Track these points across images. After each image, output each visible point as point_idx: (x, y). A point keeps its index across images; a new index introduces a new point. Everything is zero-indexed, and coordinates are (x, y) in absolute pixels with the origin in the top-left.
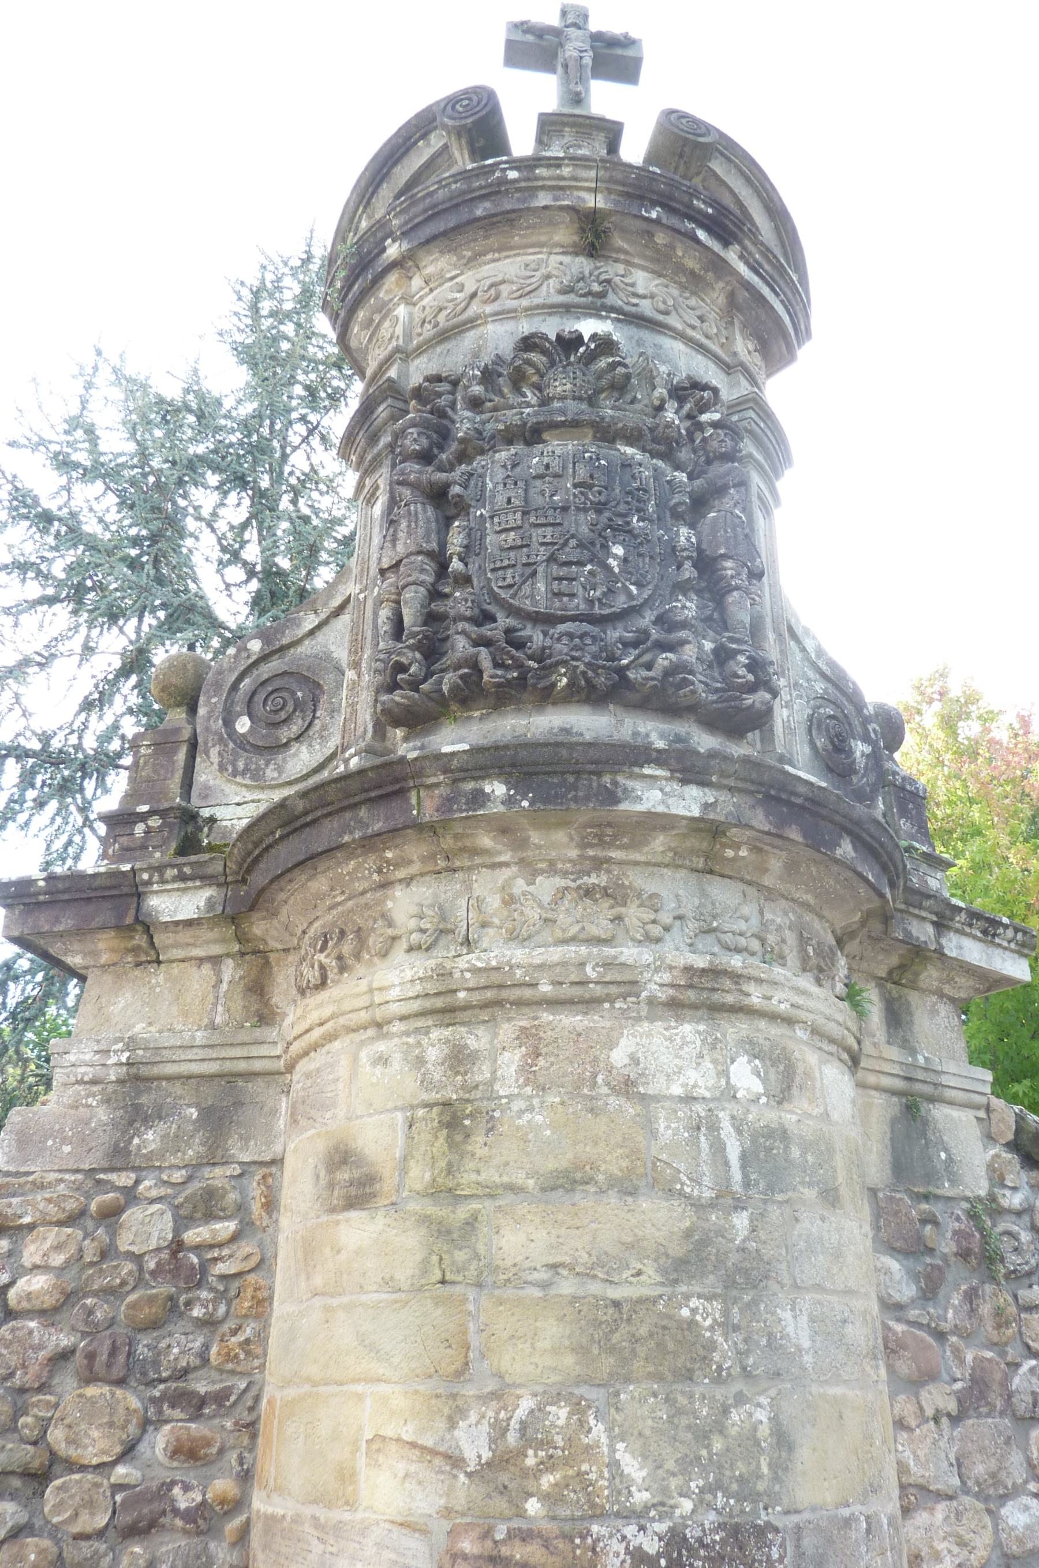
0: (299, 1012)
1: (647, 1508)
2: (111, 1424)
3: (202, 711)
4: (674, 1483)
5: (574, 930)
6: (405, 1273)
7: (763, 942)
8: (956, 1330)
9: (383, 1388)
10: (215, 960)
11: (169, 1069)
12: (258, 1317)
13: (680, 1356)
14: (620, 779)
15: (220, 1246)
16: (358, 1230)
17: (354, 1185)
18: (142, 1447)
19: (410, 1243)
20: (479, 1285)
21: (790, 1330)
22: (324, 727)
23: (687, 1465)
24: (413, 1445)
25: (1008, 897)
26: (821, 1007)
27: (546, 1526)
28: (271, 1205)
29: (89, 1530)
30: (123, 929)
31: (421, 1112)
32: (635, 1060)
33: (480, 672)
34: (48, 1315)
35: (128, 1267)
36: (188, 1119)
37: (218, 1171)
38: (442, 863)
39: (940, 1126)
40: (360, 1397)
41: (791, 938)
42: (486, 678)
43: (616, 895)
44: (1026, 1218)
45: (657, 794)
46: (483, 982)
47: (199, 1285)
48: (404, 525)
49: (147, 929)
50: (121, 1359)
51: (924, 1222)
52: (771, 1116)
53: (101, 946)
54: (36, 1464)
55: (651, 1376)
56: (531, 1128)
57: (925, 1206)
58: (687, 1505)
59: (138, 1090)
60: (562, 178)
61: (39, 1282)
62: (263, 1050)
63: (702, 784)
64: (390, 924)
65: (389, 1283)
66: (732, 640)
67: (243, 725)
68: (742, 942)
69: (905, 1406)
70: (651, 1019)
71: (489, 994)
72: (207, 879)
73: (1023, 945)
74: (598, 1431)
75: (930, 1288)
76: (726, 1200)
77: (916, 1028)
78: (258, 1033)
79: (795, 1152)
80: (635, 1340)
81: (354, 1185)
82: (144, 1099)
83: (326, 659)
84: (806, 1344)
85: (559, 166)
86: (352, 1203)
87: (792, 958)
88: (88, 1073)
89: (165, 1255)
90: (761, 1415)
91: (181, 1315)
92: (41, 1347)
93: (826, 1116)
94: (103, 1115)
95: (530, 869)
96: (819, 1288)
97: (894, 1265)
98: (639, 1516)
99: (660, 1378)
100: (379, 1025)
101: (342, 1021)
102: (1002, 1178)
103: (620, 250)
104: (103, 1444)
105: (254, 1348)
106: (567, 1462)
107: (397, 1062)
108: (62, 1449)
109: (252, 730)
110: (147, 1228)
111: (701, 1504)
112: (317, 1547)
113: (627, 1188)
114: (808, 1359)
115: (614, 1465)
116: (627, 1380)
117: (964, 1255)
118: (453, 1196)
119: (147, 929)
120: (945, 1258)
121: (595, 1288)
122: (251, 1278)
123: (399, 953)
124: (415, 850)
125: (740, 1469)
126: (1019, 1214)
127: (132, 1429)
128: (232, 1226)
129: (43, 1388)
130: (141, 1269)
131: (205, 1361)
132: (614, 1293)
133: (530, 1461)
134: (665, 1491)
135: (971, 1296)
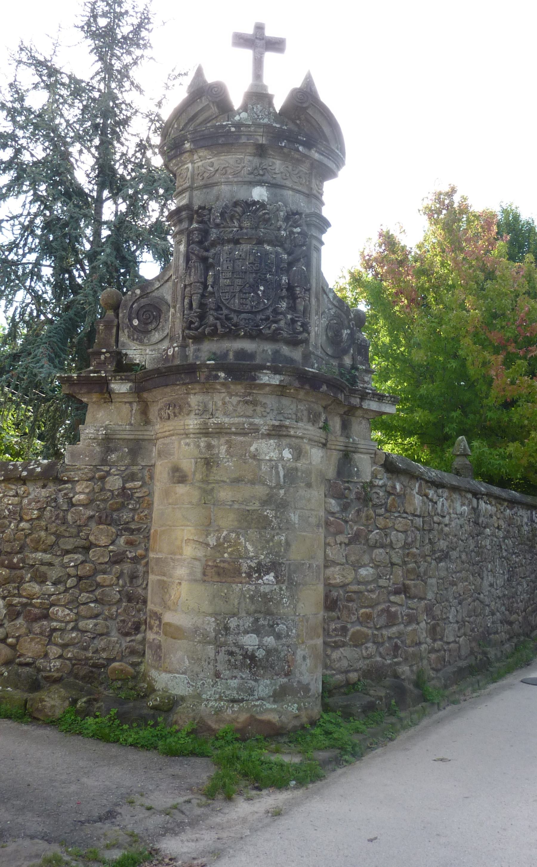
0: (161, 426)
1: (253, 557)
2: (108, 535)
3: (121, 315)
4: (260, 552)
5: (242, 413)
6: (195, 501)
7: (297, 415)
8: (352, 520)
9: (189, 528)
10: (130, 403)
11: (118, 437)
12: (148, 508)
13: (264, 524)
14: (257, 373)
15: (137, 489)
16: (181, 489)
17: (179, 476)
18: (117, 542)
19: (196, 494)
20: (214, 505)
21: (293, 519)
22: (163, 326)
23: (263, 548)
24: (197, 541)
25: (458, 326)
26: (312, 433)
27: (229, 559)
28: (151, 478)
29: (103, 562)
30: (102, 393)
31: (199, 460)
32: (256, 450)
33: (217, 329)
34: (85, 506)
35: (109, 494)
36: (125, 452)
37: (135, 467)
38: (205, 390)
39: (356, 460)
40: (183, 530)
41: (305, 413)
42: (219, 332)
43: (254, 403)
44: (384, 488)
45: (267, 378)
46: (216, 427)
47: (131, 499)
48: (193, 270)
49: (109, 393)
50: (109, 518)
51: (345, 489)
52: (294, 465)
53: (94, 396)
54: (87, 545)
55: (256, 528)
56: (229, 465)
57: (346, 485)
58: (263, 557)
59: (108, 443)
60: (250, 132)
61: (82, 497)
62: (148, 433)
63: (280, 374)
64: (190, 406)
65: (190, 503)
66: (296, 317)
67: (136, 322)
68: (290, 416)
69: (330, 540)
70: (262, 439)
71: (218, 430)
72: (130, 380)
73: (394, 402)
74: (242, 539)
75: (345, 508)
76: (279, 486)
77: (352, 429)
78: (146, 428)
79: (299, 474)
80: (252, 519)
81: (179, 476)
82: (110, 445)
83: (162, 299)
84: (297, 522)
85: (249, 127)
86: (179, 482)
87: (305, 419)
88: (93, 436)
89: (120, 491)
90: (283, 538)
91: (125, 507)
92: (84, 514)
93: (310, 463)
94: (98, 449)
95: (231, 395)
96: (302, 509)
97: (333, 501)
98: (251, 559)
99: (258, 528)
100: (187, 434)
101: (176, 432)
102: (376, 476)
103: (271, 154)
104: (105, 541)
105: (148, 517)
106: (234, 546)
107: (192, 446)
108: (94, 541)
109: (138, 324)
110: (114, 483)
111: (266, 556)
112: (172, 564)
113: (252, 482)
114: (297, 526)
115: (246, 547)
116: (250, 528)
117: (358, 499)
118: (208, 483)
119: (109, 393)
120: (352, 500)
121: (243, 507)
122: (147, 498)
123: (192, 416)
124: (198, 387)
125: (276, 549)
126: (381, 487)
127: (114, 537)
128: (140, 483)
129: (86, 525)
130: (113, 494)
131: (133, 520)
132: (248, 508)
133: (226, 545)
134: (257, 553)
135: (358, 511)
